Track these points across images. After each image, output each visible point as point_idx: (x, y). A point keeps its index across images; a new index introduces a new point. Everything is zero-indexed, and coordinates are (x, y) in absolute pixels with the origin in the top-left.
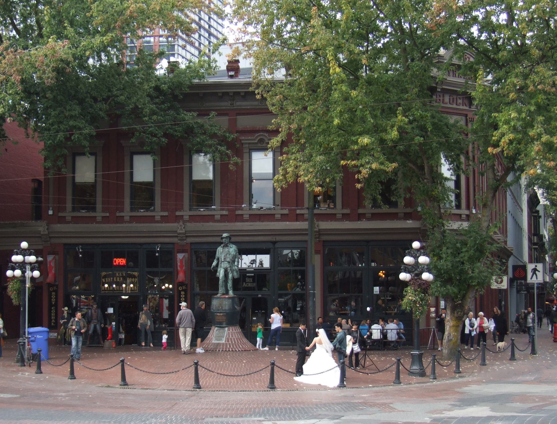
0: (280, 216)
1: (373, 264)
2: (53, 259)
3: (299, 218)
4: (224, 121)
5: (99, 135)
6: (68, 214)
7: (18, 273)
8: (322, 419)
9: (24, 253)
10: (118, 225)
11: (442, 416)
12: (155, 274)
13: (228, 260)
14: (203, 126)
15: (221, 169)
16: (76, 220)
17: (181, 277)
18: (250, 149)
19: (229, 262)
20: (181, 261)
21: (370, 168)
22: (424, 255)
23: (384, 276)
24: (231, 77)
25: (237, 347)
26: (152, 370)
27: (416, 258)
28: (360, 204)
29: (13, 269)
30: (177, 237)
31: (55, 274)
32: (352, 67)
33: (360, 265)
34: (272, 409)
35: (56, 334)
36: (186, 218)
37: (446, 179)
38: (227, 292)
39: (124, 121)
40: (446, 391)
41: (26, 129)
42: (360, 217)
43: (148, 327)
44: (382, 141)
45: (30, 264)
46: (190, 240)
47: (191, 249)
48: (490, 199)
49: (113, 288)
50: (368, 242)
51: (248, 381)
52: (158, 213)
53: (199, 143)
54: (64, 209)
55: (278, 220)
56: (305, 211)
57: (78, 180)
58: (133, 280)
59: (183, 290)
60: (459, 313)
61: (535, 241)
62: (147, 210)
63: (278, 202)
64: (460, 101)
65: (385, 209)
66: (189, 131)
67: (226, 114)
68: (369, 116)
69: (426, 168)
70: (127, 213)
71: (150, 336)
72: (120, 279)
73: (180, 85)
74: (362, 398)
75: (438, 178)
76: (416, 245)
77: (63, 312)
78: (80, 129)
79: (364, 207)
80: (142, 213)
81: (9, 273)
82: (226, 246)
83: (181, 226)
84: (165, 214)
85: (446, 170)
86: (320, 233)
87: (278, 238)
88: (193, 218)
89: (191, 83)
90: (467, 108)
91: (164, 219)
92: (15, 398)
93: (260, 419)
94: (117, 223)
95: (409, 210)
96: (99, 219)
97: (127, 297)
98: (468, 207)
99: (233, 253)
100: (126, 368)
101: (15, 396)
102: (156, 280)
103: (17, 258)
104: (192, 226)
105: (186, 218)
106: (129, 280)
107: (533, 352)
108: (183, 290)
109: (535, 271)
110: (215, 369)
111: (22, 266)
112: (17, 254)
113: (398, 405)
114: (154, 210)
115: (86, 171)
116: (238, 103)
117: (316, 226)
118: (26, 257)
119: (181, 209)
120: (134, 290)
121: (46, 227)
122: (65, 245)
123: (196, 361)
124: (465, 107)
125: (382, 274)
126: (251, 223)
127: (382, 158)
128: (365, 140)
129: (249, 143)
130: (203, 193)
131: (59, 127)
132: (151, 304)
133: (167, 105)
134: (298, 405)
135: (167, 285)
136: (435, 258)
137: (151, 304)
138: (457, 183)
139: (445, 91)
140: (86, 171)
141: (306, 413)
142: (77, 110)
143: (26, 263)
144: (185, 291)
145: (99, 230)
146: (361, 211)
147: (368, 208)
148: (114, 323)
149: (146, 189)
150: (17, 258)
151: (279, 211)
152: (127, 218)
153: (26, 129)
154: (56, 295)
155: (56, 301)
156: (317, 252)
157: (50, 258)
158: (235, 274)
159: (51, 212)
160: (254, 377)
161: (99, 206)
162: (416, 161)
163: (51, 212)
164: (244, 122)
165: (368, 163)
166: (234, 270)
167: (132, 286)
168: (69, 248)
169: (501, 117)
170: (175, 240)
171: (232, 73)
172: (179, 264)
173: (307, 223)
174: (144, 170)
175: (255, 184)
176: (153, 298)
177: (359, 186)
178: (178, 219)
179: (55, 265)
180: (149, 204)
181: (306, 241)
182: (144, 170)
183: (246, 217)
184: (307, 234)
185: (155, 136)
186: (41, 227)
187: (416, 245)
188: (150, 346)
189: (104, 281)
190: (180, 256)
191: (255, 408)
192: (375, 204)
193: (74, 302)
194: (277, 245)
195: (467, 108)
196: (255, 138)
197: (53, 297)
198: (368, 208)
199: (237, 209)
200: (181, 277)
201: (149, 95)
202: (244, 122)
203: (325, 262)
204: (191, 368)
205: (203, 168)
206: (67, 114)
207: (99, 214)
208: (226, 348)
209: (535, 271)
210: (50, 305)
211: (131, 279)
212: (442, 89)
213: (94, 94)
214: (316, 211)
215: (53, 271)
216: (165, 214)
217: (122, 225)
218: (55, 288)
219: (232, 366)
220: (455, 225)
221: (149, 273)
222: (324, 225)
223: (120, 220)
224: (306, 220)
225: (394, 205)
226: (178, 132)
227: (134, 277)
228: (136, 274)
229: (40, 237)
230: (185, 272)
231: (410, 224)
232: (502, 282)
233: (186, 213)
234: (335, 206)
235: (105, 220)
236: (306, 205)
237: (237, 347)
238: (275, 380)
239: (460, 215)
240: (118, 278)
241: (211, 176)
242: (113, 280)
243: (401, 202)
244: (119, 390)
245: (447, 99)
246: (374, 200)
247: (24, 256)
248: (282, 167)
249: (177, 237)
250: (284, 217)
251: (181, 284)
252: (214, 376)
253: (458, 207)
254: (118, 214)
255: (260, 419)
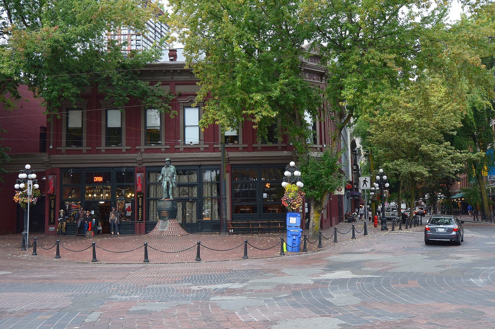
0: (203, 149)
1: (263, 179)
2: (52, 178)
3: (215, 150)
4: (167, 89)
5: (83, 96)
6: (64, 148)
7: (22, 185)
8: (235, 283)
9: (28, 172)
10: (97, 155)
11: (320, 278)
12: (122, 187)
13: (169, 175)
14: (153, 91)
15: (165, 118)
16: (68, 152)
17: (139, 188)
18: (184, 107)
19: (170, 177)
20: (139, 178)
21: (262, 115)
22: (297, 170)
23: (269, 187)
24: (171, 60)
25: (175, 233)
26: (116, 250)
27: (292, 172)
28: (254, 142)
29: (20, 183)
30: (136, 162)
31: (54, 188)
32: (249, 52)
33: (254, 180)
34: (198, 276)
35: (54, 228)
36: (143, 150)
37: (308, 125)
38: (169, 197)
39: (100, 86)
40: (317, 260)
41: (34, 92)
42: (254, 149)
43: (116, 222)
44: (270, 98)
45: (32, 179)
46: (145, 165)
47: (146, 170)
48: (338, 135)
49: (94, 197)
50: (259, 165)
51: (182, 256)
52: (124, 148)
53: (151, 101)
54: (140, 145)
55: (202, 152)
56: (219, 146)
57: (71, 125)
58: (107, 191)
59: (140, 197)
60: (319, 209)
61: (355, 169)
62: (117, 144)
63: (202, 138)
64: (315, 77)
65: (271, 144)
66: (145, 94)
67: (169, 84)
68: (260, 81)
69: (297, 115)
70: (103, 147)
71: (117, 228)
72: (98, 191)
73: (137, 65)
74: (260, 266)
75: (303, 123)
76: (292, 164)
77: (60, 213)
78: (68, 89)
79: (257, 143)
80: (113, 147)
81: (17, 186)
82: (168, 166)
83: (139, 155)
84: (129, 148)
85: (308, 118)
86: (229, 159)
87: (203, 163)
88: (147, 151)
89: (145, 63)
90: (319, 82)
91: (128, 151)
92: (8, 274)
93: (189, 284)
94: (96, 154)
95: (284, 145)
96: (84, 151)
97: (103, 202)
98: (321, 143)
99: (172, 171)
100: (97, 250)
101: (9, 273)
102: (123, 191)
103: (22, 176)
104: (146, 156)
105: (143, 150)
106: (104, 191)
107: (366, 233)
108: (140, 197)
109: (365, 181)
110: (160, 248)
111: (25, 181)
112: (23, 173)
113: (285, 271)
114: (121, 146)
115: (75, 120)
116: (176, 77)
117: (226, 155)
118: (29, 175)
119: (139, 144)
120: (108, 198)
121: (48, 157)
122: (61, 168)
123: (145, 243)
124: (318, 81)
125: (268, 186)
126: (185, 154)
127: (269, 108)
128: (258, 97)
129: (183, 103)
130: (153, 136)
131: (54, 87)
132: (120, 207)
133: (130, 76)
134: (217, 272)
135: (130, 194)
136: (304, 173)
137: (120, 207)
138: (314, 127)
139: (306, 71)
140: (75, 120)
141: (222, 278)
142: (67, 76)
143: (29, 179)
144: (142, 197)
145: (85, 159)
146: (254, 145)
147: (259, 144)
148: (94, 220)
149: (117, 131)
150: (22, 176)
151: (203, 146)
152: (103, 151)
153: (34, 92)
154: (55, 202)
155: (55, 206)
156: (227, 172)
157: (50, 177)
158: (174, 184)
159: (51, 147)
160: (186, 253)
161: (84, 141)
162: (289, 111)
163: (51, 147)
164: (180, 89)
165: (260, 112)
166: (173, 182)
167: (107, 195)
168: (64, 171)
169: (346, 81)
170: (135, 165)
171: (172, 58)
172: (138, 180)
173: (221, 153)
174: (114, 119)
175: (187, 129)
176: (121, 202)
177: (254, 127)
178: (137, 151)
179: (54, 181)
180: (118, 142)
181: (220, 165)
182: (114, 119)
183: (182, 149)
184: (220, 160)
185: (121, 96)
186: (45, 157)
187: (292, 164)
188: (117, 234)
189: (87, 192)
190: (138, 175)
191: (186, 276)
192: (264, 142)
193: (67, 206)
194: (202, 168)
195: (319, 82)
196: (187, 99)
197: (140, 201)
198: (259, 144)
199: (175, 144)
200: (139, 188)
201: (117, 69)
202: (180, 89)
203: (232, 178)
204: (188, 252)
205: (154, 119)
206: (60, 79)
207: (84, 148)
208: (168, 234)
209: (365, 181)
210: (50, 208)
211: (106, 190)
212: (304, 69)
213: (80, 67)
214: (226, 146)
215: (52, 186)
216: (129, 148)
217: (100, 155)
218: (54, 197)
219: (171, 246)
220: (314, 154)
221: (119, 186)
222: (232, 154)
223: (99, 152)
224: (220, 151)
225: (276, 141)
226: (137, 93)
227: (107, 189)
228: (109, 187)
229: (44, 163)
230: (142, 186)
231: (285, 153)
232: (341, 190)
233: (143, 147)
234: (238, 142)
235: (89, 152)
236: (220, 141)
237: (175, 233)
238: (201, 255)
239: (316, 148)
240: (97, 190)
241: (158, 123)
242: (94, 191)
243: (280, 139)
244: (91, 265)
245: (307, 76)
246: (263, 137)
247: (28, 174)
248: (204, 114)
249: (136, 162)
250: (206, 150)
251: (140, 193)
252: (159, 253)
253: (315, 143)
254: (97, 148)
255: (189, 284)
